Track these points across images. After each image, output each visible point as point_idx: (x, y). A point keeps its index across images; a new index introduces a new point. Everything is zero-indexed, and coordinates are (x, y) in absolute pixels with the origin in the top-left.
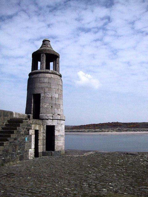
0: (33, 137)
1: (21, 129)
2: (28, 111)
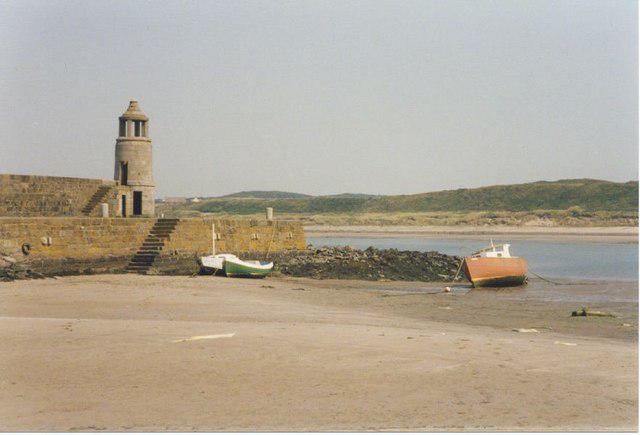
0: (121, 200)
1: (110, 194)
2: (116, 178)
